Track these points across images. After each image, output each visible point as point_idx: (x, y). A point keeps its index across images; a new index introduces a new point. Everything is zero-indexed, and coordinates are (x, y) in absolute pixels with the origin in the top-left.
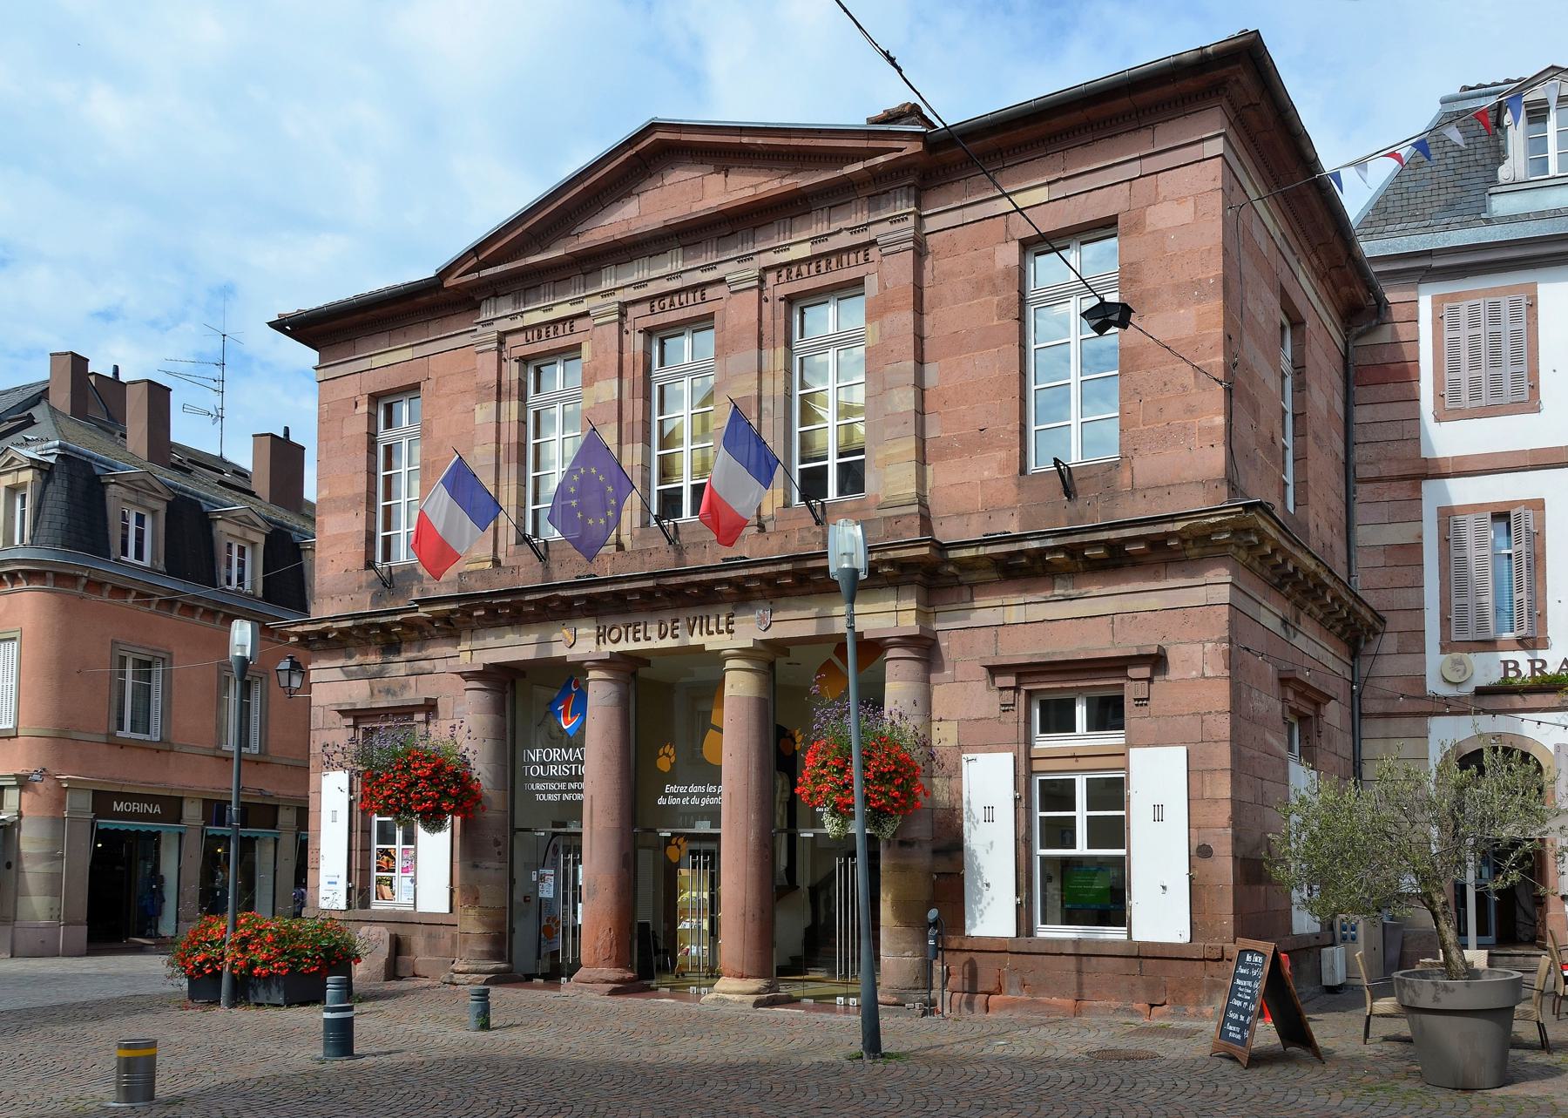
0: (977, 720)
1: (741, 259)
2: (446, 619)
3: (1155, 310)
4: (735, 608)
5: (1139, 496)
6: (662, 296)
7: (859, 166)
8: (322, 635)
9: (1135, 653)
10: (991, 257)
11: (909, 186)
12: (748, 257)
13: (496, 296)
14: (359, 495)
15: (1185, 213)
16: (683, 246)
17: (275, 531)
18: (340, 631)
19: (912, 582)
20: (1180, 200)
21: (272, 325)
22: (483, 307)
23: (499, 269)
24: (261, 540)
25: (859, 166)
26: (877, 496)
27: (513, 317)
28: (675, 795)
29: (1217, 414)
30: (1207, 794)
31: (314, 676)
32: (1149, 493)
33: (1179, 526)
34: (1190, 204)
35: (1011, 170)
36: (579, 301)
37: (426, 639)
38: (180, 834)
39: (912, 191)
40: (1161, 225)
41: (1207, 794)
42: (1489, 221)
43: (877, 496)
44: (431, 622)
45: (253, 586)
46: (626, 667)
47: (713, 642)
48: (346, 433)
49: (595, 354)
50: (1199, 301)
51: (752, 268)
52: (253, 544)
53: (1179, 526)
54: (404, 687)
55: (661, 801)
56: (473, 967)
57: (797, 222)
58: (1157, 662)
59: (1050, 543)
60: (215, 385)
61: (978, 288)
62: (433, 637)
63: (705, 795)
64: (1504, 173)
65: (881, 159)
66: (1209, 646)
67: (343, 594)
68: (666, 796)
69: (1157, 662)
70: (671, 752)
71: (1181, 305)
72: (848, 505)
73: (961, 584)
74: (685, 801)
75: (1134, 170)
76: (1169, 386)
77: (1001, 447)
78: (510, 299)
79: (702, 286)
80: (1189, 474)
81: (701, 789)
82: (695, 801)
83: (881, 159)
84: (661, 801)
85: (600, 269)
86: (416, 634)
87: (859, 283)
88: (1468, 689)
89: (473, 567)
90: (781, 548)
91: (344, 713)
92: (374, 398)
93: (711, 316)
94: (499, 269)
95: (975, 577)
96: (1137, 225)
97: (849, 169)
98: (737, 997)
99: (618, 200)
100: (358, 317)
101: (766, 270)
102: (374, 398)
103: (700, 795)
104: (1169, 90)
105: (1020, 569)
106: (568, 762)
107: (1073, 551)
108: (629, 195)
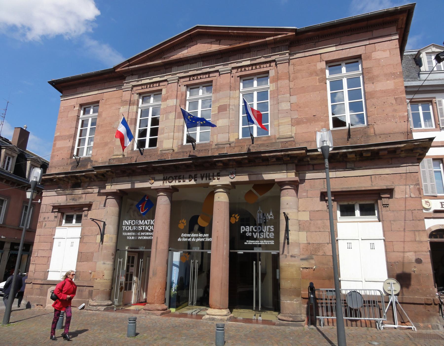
0: (318, 211)
1: (224, 65)
2: (103, 175)
3: (378, 81)
4: (221, 171)
5: (378, 137)
6: (194, 75)
7: (272, 38)
8: (51, 180)
9: (385, 188)
10: (315, 66)
11: (286, 45)
12: (227, 64)
13: (132, 75)
14: (71, 135)
15: (387, 54)
16: (203, 61)
17: (21, 154)
18: (59, 179)
19: (293, 163)
20: (384, 51)
21: (49, 82)
22: (127, 78)
23: (136, 66)
24: (16, 156)
25: (272, 38)
26: (275, 136)
27: (138, 81)
28: (185, 238)
29: (405, 112)
30: (417, 239)
31: (44, 194)
32: (381, 136)
33: (402, 145)
34: (388, 52)
35: (321, 42)
36: (163, 76)
37: (92, 181)
38: (362, 240)
39: (287, 47)
40: (378, 57)
41: (417, 239)
42: (420, 80)
43: (275, 136)
44: (96, 175)
45: (11, 170)
46: (171, 192)
47: (215, 182)
48: (69, 116)
49: (167, 92)
50: (394, 79)
51: (229, 67)
52: (13, 157)
53: (402, 145)
54: (80, 198)
55: (179, 240)
56: (99, 304)
57: (245, 55)
58: (390, 192)
59: (350, 150)
60: (2, 115)
61: (311, 74)
62: (94, 181)
63: (198, 237)
64: (422, 69)
65: (280, 36)
66: (412, 186)
67: (60, 166)
68: (182, 238)
69: (390, 192)
70: (238, 217)
71: (387, 80)
72: (263, 138)
73: (309, 164)
74: (189, 240)
75: (367, 42)
76: (385, 104)
77: (322, 121)
78: (137, 76)
79: (209, 73)
80: (397, 130)
81: (197, 235)
82: (193, 240)
83: (280, 36)
84: (179, 240)
85: (171, 68)
86: (88, 179)
87: (268, 72)
88: (431, 211)
89: (115, 157)
90: (239, 151)
91: (54, 207)
92: (81, 105)
93: (211, 81)
94: (136, 66)
95: (315, 162)
96: (369, 57)
97: (267, 39)
98: (219, 317)
99: (180, 48)
100: (80, 81)
101: (233, 68)
102: (81, 105)
103: (196, 238)
104: (381, 20)
105: (339, 159)
106: (142, 225)
107: (360, 154)
108: (184, 47)
